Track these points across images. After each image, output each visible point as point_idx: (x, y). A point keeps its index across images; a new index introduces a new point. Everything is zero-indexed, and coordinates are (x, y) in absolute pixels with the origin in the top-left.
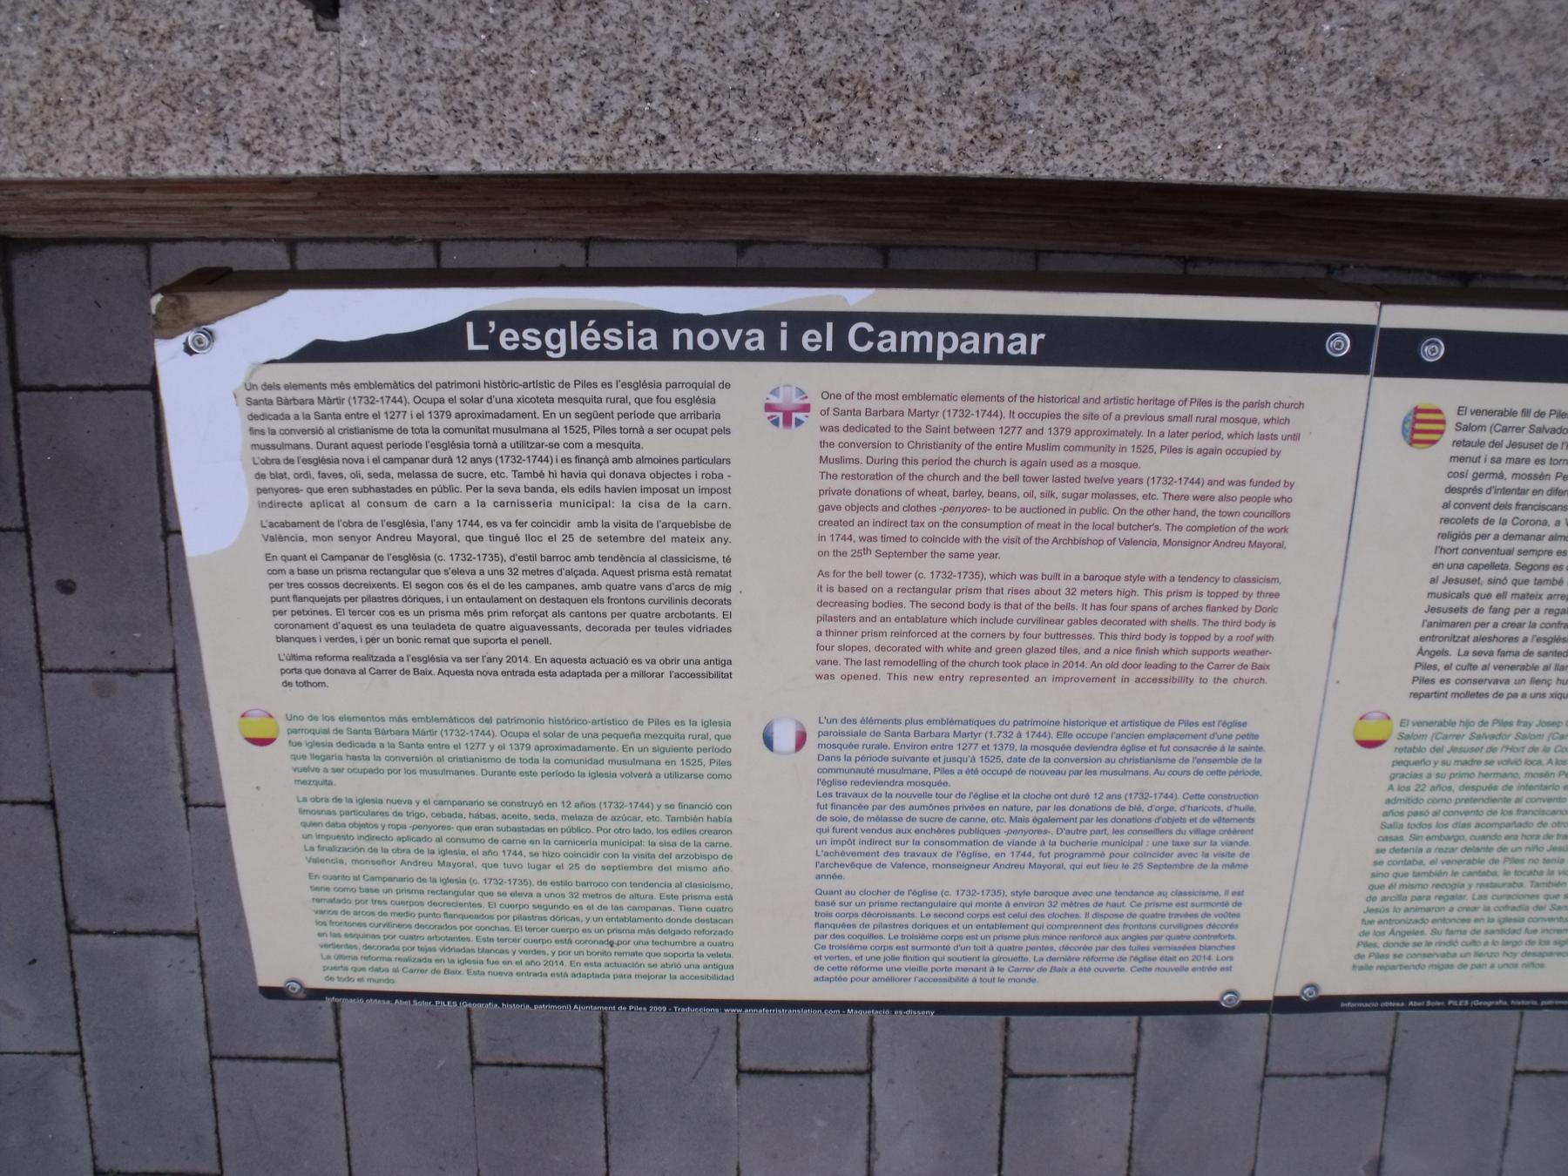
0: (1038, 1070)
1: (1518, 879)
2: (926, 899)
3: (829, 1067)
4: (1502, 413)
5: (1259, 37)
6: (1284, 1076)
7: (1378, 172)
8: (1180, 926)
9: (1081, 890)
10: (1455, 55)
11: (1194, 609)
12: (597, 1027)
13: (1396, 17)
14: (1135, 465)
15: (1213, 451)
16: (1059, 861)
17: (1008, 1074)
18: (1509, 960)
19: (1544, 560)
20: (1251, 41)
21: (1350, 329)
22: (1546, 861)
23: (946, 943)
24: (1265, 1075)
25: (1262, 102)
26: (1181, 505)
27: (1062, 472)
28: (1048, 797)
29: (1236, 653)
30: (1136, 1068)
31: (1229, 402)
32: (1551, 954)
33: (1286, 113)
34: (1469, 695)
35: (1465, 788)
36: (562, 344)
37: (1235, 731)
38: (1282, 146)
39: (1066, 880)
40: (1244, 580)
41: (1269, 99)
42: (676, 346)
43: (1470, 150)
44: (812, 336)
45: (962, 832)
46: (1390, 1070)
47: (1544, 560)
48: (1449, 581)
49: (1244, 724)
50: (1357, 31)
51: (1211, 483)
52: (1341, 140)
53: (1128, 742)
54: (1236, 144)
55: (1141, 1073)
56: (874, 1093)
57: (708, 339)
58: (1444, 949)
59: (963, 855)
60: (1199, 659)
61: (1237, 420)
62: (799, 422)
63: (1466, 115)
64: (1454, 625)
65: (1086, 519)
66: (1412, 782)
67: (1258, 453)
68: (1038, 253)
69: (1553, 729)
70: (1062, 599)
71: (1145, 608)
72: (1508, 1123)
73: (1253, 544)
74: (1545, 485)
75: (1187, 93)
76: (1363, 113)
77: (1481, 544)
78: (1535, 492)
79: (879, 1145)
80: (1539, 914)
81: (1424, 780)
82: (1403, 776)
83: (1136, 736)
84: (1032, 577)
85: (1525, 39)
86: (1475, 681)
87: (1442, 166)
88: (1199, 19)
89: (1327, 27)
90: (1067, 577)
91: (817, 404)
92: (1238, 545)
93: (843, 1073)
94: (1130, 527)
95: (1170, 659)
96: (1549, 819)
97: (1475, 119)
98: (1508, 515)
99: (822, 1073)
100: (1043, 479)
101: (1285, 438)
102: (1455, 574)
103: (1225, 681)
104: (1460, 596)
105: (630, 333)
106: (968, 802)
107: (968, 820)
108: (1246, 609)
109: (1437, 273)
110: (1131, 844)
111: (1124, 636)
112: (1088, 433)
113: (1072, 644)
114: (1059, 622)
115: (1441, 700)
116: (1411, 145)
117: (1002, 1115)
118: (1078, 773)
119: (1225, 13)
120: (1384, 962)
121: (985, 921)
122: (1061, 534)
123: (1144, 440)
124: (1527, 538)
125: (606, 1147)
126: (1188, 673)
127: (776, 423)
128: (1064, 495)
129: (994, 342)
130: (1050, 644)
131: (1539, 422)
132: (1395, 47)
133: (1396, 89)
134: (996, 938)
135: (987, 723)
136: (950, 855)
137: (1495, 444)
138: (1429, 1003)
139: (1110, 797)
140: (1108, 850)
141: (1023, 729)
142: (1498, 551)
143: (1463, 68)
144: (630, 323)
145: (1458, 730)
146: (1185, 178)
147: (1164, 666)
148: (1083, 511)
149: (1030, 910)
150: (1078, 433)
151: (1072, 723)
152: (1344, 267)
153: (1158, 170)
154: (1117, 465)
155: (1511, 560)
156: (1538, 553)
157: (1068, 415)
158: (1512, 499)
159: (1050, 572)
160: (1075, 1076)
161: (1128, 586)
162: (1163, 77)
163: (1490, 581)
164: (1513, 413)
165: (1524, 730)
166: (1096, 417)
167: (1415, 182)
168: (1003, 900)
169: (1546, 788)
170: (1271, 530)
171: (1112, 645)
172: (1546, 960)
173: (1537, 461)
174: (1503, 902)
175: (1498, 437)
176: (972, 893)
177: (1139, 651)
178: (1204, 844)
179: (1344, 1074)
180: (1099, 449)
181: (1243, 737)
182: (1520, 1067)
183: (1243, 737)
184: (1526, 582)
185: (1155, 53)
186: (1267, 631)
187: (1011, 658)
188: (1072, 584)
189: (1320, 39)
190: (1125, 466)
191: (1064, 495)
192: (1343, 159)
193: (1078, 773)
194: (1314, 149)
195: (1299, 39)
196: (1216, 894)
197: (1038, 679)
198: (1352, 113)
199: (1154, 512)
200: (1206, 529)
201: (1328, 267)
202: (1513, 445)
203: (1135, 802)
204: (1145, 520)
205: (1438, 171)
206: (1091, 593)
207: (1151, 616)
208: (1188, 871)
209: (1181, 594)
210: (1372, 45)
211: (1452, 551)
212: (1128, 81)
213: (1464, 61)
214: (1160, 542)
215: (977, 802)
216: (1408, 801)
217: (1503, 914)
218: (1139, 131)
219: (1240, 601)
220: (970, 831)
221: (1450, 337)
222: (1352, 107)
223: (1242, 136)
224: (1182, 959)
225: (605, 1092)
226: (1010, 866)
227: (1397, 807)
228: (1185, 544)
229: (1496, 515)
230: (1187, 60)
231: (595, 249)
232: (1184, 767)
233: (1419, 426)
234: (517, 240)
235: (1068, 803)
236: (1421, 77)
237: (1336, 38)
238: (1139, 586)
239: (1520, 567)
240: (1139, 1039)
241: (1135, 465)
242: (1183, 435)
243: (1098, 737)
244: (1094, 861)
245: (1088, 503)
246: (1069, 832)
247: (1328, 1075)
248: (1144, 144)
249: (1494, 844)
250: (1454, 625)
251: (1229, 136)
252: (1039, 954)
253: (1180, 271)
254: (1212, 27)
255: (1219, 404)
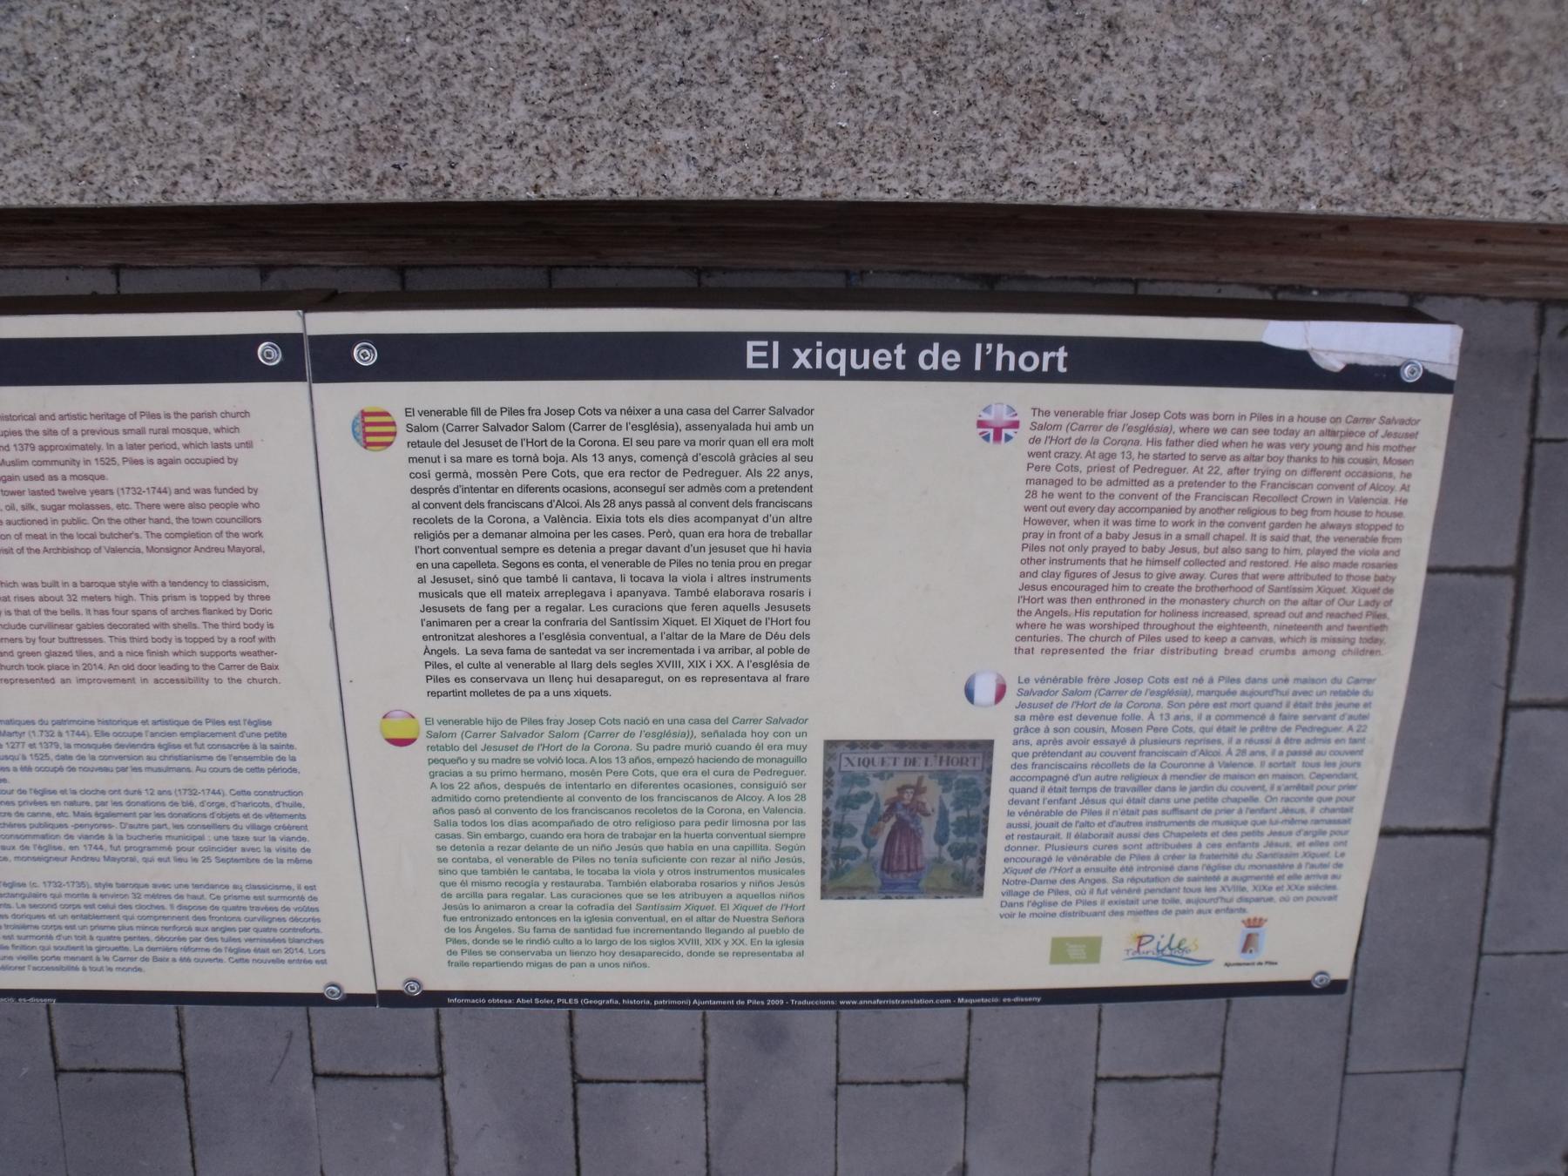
0: (605, 1076)
1: (595, 878)
2: (15, 890)
3: (401, 1070)
4: (451, 413)
5: (130, 62)
6: (858, 1084)
7: (249, 186)
8: (263, 919)
9: (160, 882)
10: (312, 68)
11: (192, 612)
12: (175, 1031)
13: (255, 35)
14: (102, 477)
15: (172, 462)
16: (131, 854)
17: (578, 1080)
18: (608, 959)
19: (530, 557)
20: (123, 66)
21: (278, 339)
22: (617, 860)
23: (49, 932)
24: (838, 1083)
25: (138, 125)
26: (155, 514)
27: (37, 485)
28: (103, 792)
29: (243, 654)
30: (705, 1074)
31: (177, 414)
32: (651, 954)
33: (160, 133)
34: (487, 693)
35: (509, 786)
36: (842, 365)
37: (262, 729)
38: (160, 166)
39: (127, 872)
40: (232, 584)
41: (144, 121)
42: (999, 367)
43: (333, 159)
44: (883, 355)
45: (32, 826)
46: (966, 1078)
47: (530, 557)
48: (437, 580)
49: (269, 723)
50: (220, 50)
51: (178, 491)
52: (213, 157)
53: (164, 741)
54: (117, 167)
55: (711, 1080)
56: (448, 1097)
57: (1029, 361)
58: (538, 948)
59: (40, 848)
60: (209, 661)
61: (189, 431)
62: (1008, 438)
63: (326, 125)
64: (454, 624)
65: (69, 529)
66: (455, 780)
67: (216, 461)
68: (550, 269)
69: (587, 728)
70: (67, 605)
71: (145, 612)
72: (1094, 1130)
73: (232, 549)
74: (515, 482)
75: (70, 120)
76: (230, 129)
77: (461, 543)
78: (505, 490)
79: (457, 1148)
80: (626, 914)
81: (465, 779)
82: (443, 774)
83: (170, 735)
84: (33, 585)
85: (375, 49)
86: (491, 680)
87: (308, 176)
88: (74, 46)
89: (192, 49)
90: (65, 584)
91: (1026, 419)
92: (217, 550)
93: (415, 1077)
94: (112, 536)
95: (181, 660)
96: (611, 818)
97: (336, 129)
98: (484, 513)
99: (394, 1077)
100: (20, 493)
101: (239, 446)
102: (441, 573)
103: (239, 681)
104: (453, 595)
105: (819, 352)
106: (31, 797)
107: (34, 815)
108: (241, 612)
109: (961, 276)
110: (194, 838)
111: (132, 639)
112: (52, 448)
113: (86, 647)
114: (69, 627)
115: (460, 699)
116: (278, 158)
117: (576, 1119)
118: (124, 770)
119: (97, 40)
120: (478, 959)
121: (77, 912)
122: (50, 543)
123: (105, 453)
124: (508, 535)
125: (192, 1151)
126: (202, 673)
127: (986, 438)
128: (44, 508)
129: (860, 360)
130: (66, 647)
131: (492, 420)
132: (255, 64)
133: (261, 105)
134: (93, 928)
135: (27, 722)
136: (27, 848)
137: (452, 444)
138: (537, 1001)
139: (161, 793)
140: (174, 844)
141: (63, 728)
142: (481, 550)
143: (321, 82)
144: (819, 344)
145: (486, 728)
146: (74, 202)
147: (176, 667)
148: (65, 522)
149: (118, 901)
150: (42, 448)
151: (107, 722)
152: (862, 273)
153: (51, 196)
154: (86, 477)
155: (498, 558)
156: (524, 551)
157: (28, 432)
158: (483, 497)
159: (49, 580)
160: (645, 1082)
161: (124, 591)
162: (47, 105)
163: (480, 580)
164: (463, 413)
165: (557, 729)
166: (55, 433)
167: (284, 193)
168: (90, 892)
169: (596, 786)
170: (246, 535)
171: (124, 647)
172: (647, 959)
173: (499, 459)
174: (585, 901)
175: (454, 436)
176: (59, 885)
177: (150, 653)
178: (263, 839)
179: (919, 1082)
180: (64, 463)
181: (271, 735)
182: (1102, 1073)
183: (271, 735)
184: (519, 580)
185: (37, 82)
186: (266, 632)
187: (33, 661)
188: (72, 590)
189: (186, 61)
190: (93, 478)
191: (44, 508)
192: (216, 176)
193: (124, 770)
194: (189, 167)
195: (167, 62)
196: (289, 887)
197: (63, 681)
198: (222, 130)
199: (131, 520)
200: (185, 536)
201: (847, 273)
202: (469, 444)
203: (187, 798)
204: (124, 529)
205: (304, 181)
206: (92, 598)
207: (153, 619)
208: (254, 865)
209: (176, 598)
210: (235, 63)
211: (433, 551)
212: (16, 112)
213: (320, 74)
214: (143, 549)
215: (39, 798)
216: (455, 798)
217: (589, 913)
218: (29, 159)
219: (232, 604)
220: (40, 826)
221: (380, 341)
222: (220, 125)
223: (123, 159)
224: (275, 951)
225: (187, 1096)
226: (86, 859)
227: (446, 805)
228: (168, 550)
229: (470, 513)
230: (67, 88)
231: (274, 276)
232: (221, 764)
233: (369, 429)
234: (50, 268)
235: (123, 798)
236: (281, 91)
237: (201, 58)
238: (134, 592)
239: (508, 565)
240: (705, 1046)
241: (102, 477)
242: (141, 447)
243: (134, 735)
244: (164, 854)
245: (68, 514)
246: (132, 827)
247: (903, 1082)
248: (34, 170)
249: (560, 843)
250: (454, 624)
251: (111, 160)
252: (138, 944)
253: (693, 283)
254: (87, 55)
255: (168, 416)
